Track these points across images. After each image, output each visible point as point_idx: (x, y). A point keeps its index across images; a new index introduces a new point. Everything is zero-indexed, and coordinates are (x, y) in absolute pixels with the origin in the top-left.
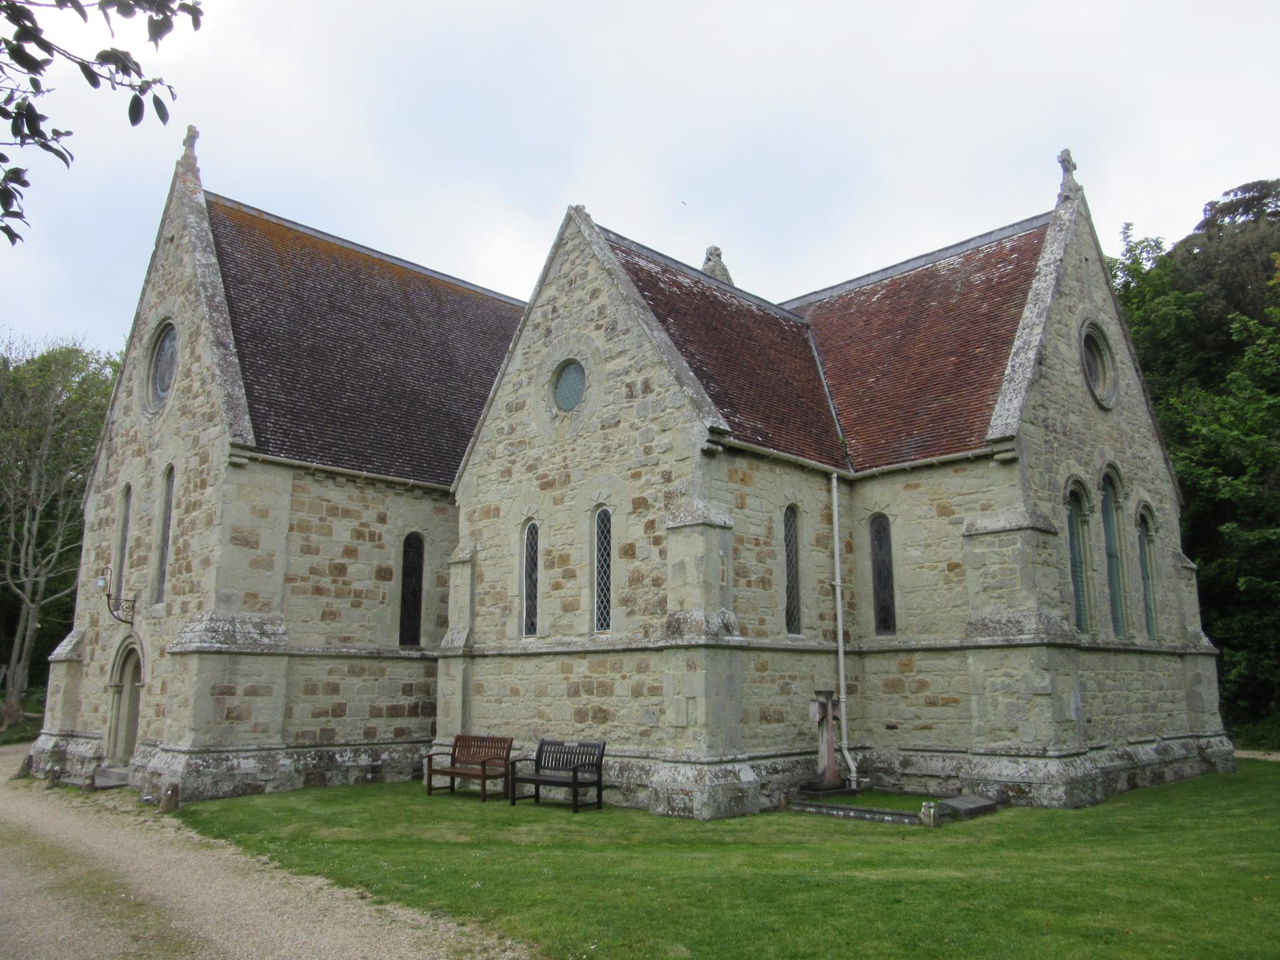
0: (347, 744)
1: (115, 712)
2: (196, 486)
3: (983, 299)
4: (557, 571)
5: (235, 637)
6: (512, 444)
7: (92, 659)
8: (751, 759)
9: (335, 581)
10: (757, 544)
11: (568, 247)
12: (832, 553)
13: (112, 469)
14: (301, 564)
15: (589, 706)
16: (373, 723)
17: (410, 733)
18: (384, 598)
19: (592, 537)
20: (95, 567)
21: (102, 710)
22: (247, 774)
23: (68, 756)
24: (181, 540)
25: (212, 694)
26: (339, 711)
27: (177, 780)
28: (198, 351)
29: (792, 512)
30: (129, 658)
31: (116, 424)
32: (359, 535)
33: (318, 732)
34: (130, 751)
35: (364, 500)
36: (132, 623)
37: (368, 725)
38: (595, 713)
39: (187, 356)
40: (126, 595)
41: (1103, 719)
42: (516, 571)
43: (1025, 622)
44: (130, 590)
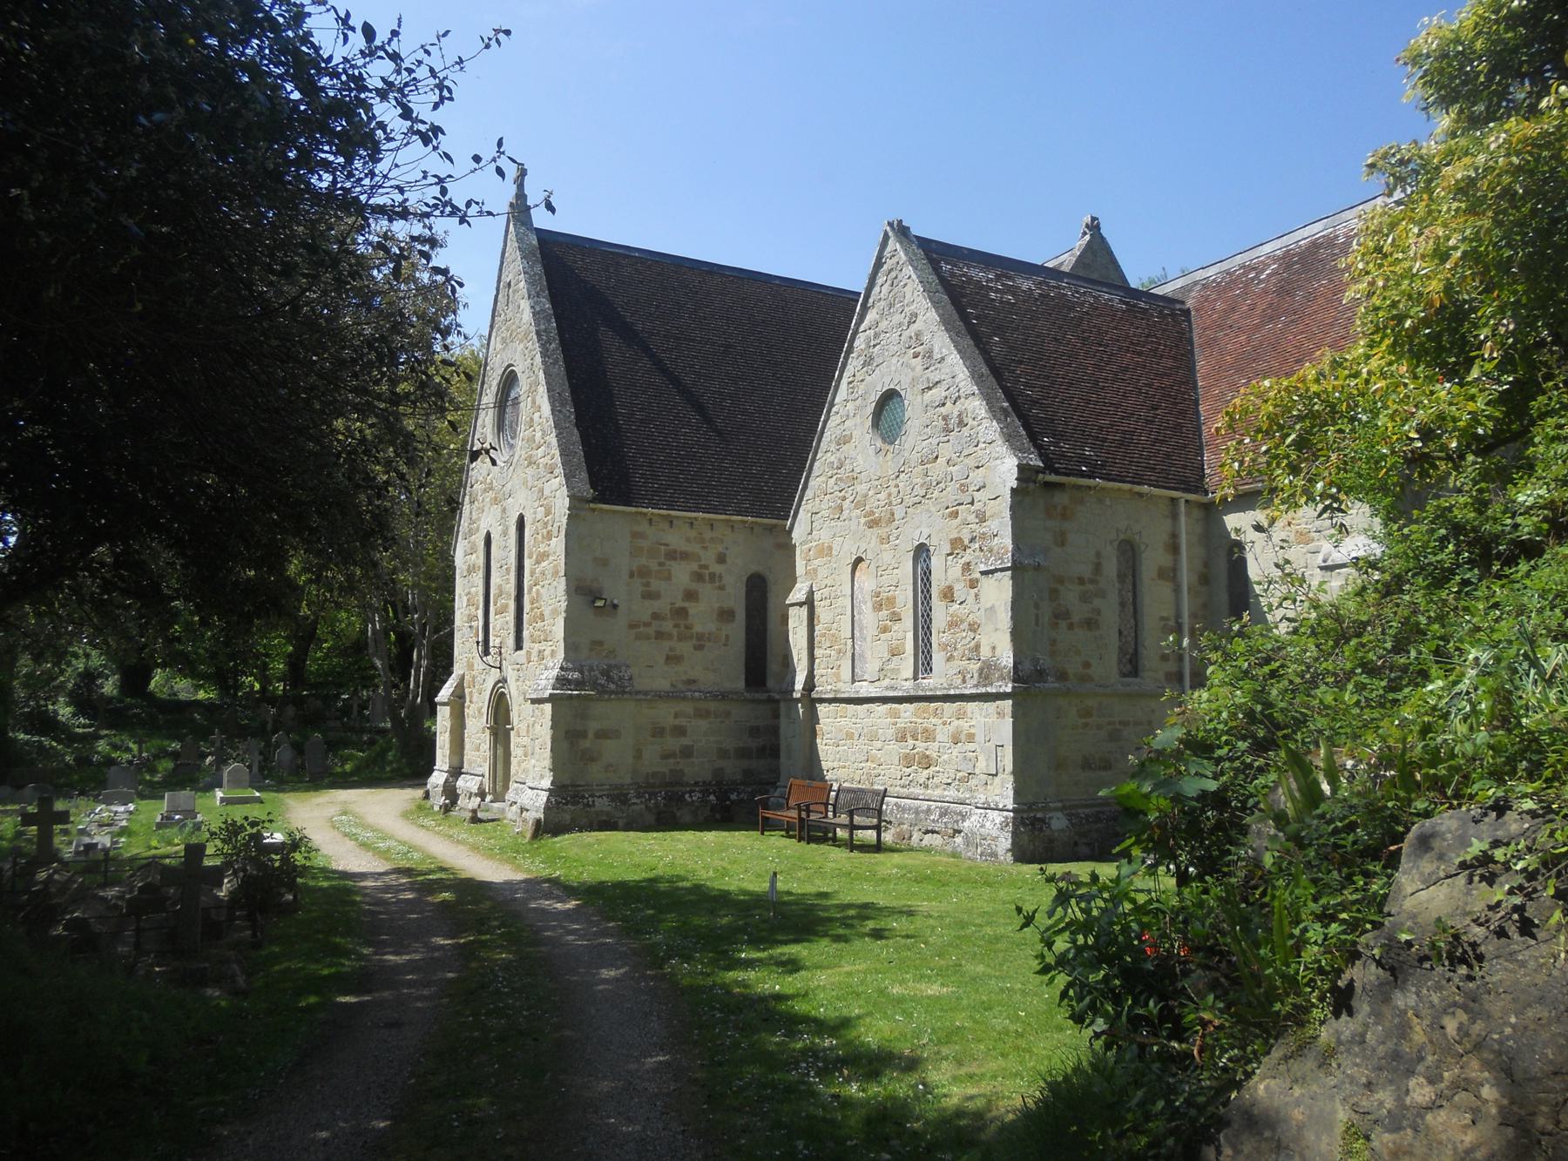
9: (676, 626)
14: (645, 610)
26: (687, 752)
32: (698, 577)
34: (506, 787)
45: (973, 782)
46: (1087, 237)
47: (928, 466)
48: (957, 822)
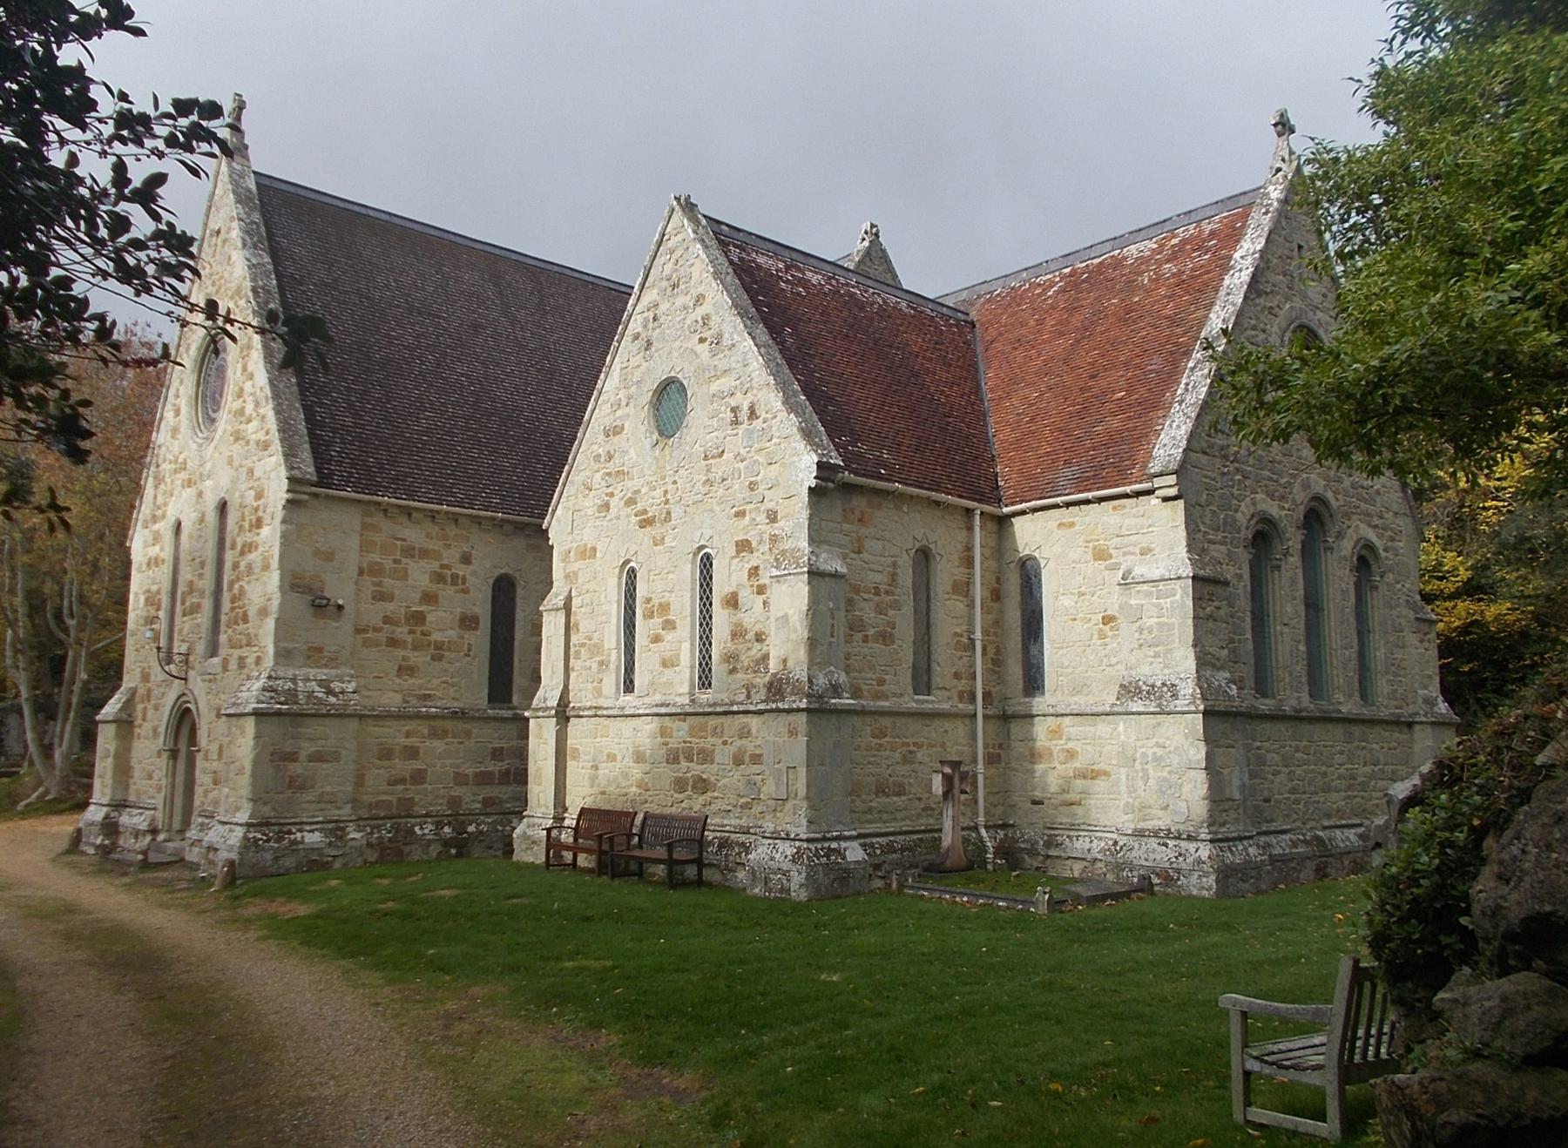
0: (427, 815)
1: (170, 780)
2: (251, 525)
3: (1171, 297)
4: (657, 621)
5: (296, 696)
6: (609, 474)
7: (144, 719)
8: (859, 836)
9: (412, 632)
10: (877, 594)
11: (670, 244)
12: (973, 601)
13: (160, 500)
14: (373, 613)
15: (689, 775)
16: (458, 791)
17: (501, 802)
18: (469, 650)
19: (693, 584)
20: (145, 614)
21: (156, 777)
22: (312, 849)
23: (121, 829)
24: (236, 586)
25: (271, 761)
26: (419, 777)
27: (234, 856)
28: (251, 368)
29: (924, 556)
30: (184, 720)
31: (164, 449)
32: (439, 578)
33: (395, 801)
34: (186, 824)
35: (445, 537)
36: (185, 679)
37: (453, 794)
38: (695, 783)
39: (239, 373)
40: (179, 647)
41: (1288, 799)
42: (614, 620)
43: (1181, 685)
44: (183, 641)
45: (757, 809)
46: (866, 243)
47: (711, 461)
48: (739, 854)
